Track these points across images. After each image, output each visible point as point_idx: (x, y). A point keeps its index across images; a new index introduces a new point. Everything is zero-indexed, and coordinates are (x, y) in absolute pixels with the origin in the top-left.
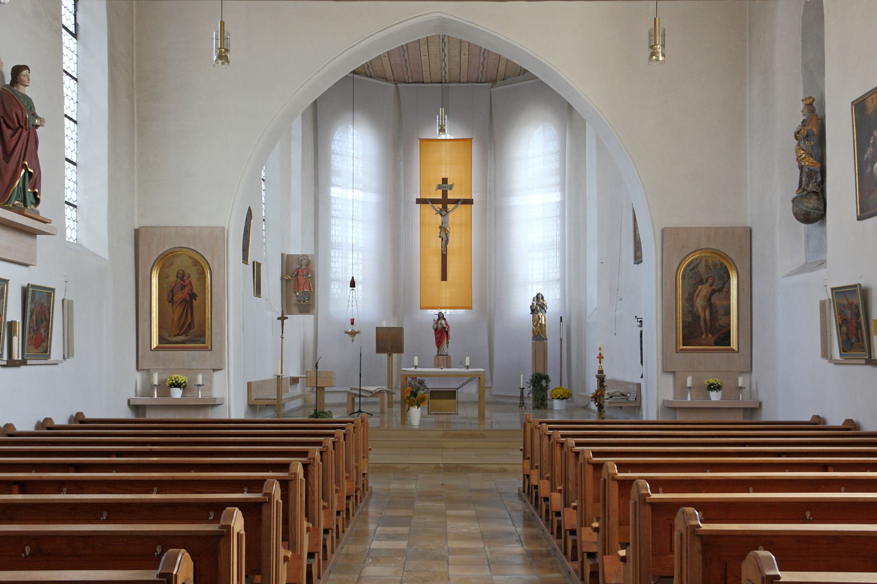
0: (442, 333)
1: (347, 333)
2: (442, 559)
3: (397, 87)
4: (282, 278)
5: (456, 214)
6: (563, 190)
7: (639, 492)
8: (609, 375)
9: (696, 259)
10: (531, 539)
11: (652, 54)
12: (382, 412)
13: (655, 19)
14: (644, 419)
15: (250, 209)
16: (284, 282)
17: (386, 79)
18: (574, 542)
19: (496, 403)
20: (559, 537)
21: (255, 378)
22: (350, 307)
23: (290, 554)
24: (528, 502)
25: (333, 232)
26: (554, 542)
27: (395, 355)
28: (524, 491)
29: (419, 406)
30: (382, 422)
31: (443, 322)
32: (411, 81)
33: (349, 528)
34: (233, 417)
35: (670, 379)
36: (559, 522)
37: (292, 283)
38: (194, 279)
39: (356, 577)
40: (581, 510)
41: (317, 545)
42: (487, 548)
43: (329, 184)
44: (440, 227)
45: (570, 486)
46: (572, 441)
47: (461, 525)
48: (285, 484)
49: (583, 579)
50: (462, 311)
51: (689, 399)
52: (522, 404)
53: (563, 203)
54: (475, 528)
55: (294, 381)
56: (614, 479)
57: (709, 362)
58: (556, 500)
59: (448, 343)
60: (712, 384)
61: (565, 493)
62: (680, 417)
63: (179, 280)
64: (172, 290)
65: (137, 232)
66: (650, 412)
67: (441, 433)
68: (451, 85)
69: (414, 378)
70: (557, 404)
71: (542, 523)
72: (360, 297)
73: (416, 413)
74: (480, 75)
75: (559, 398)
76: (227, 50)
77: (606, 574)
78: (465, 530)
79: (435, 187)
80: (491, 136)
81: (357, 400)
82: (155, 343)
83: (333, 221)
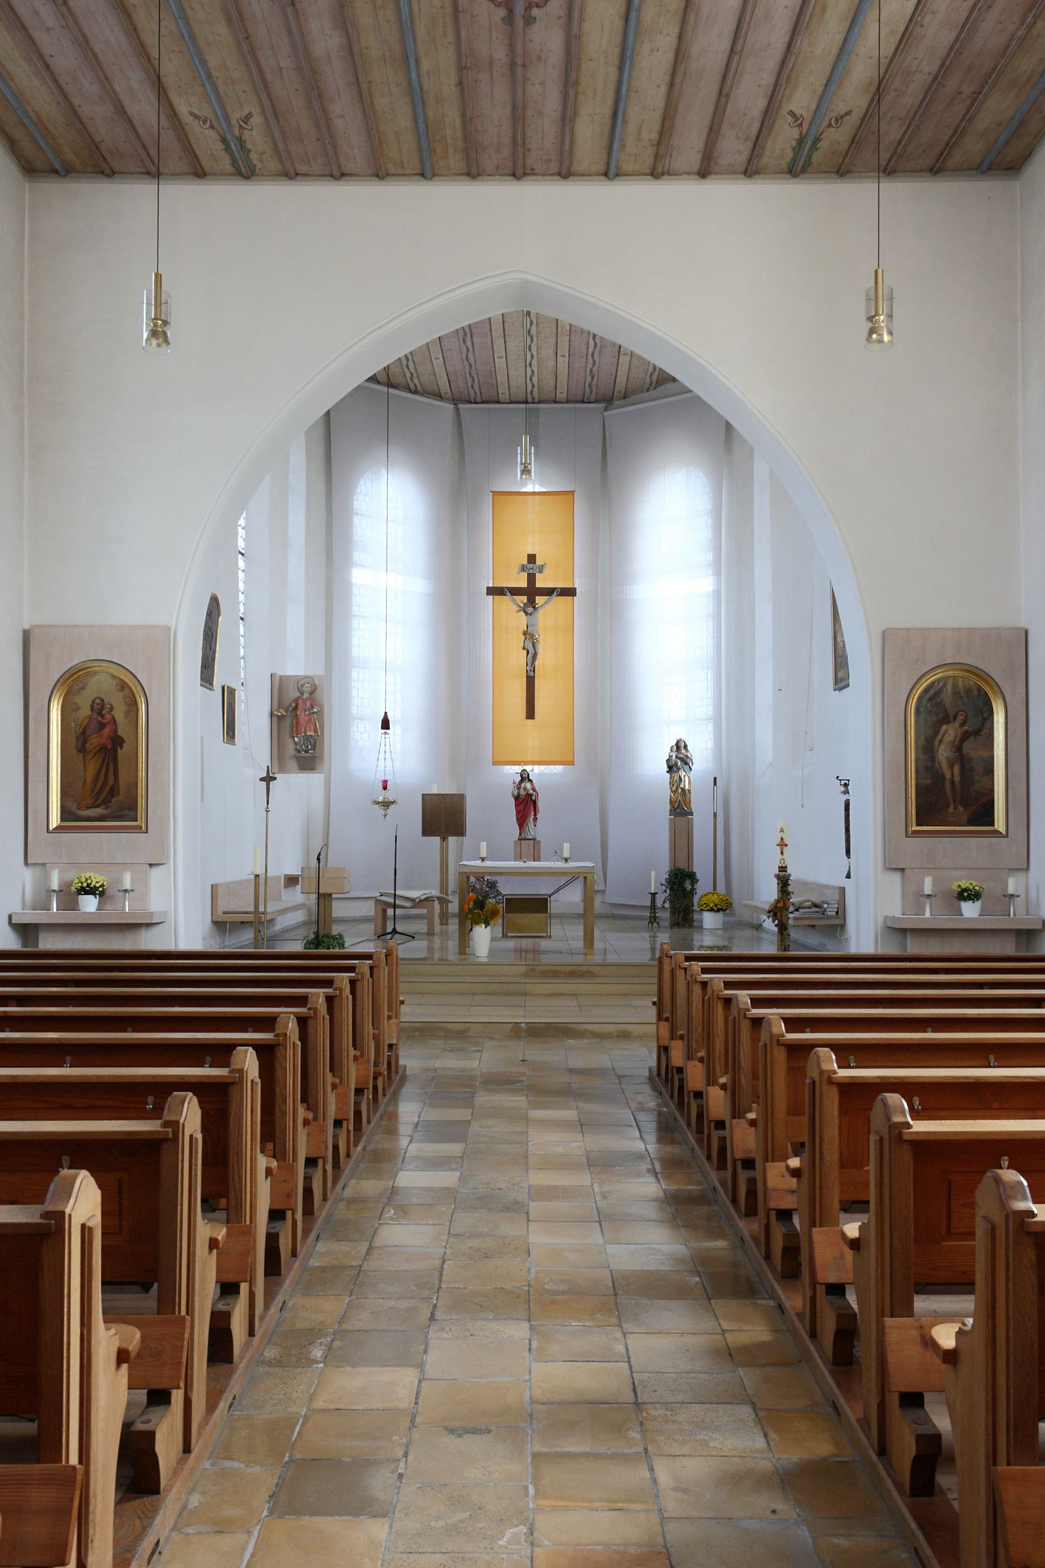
0: (526, 804)
1: (377, 803)
2: (516, 1208)
3: (457, 410)
4: (272, 714)
5: (549, 610)
6: (717, 573)
7: (889, 1119)
8: (795, 873)
9: (939, 680)
10: (671, 1166)
11: (872, 331)
12: (431, 933)
13: (876, 272)
14: (853, 949)
15: (214, 601)
16: (275, 719)
17: (439, 396)
18: (752, 1182)
19: (613, 917)
20: (721, 1166)
21: (224, 876)
22: (382, 760)
23: (221, 1234)
24: (667, 1096)
25: (355, 641)
26: (714, 1176)
27: (452, 840)
28: (659, 1074)
29: (487, 924)
30: (430, 949)
31: (528, 785)
32: (479, 400)
33: (360, 1148)
34: (183, 946)
35: (896, 878)
36: (723, 1140)
37: (288, 721)
38: (119, 714)
39: (364, 1247)
40: (764, 1126)
41: (290, 1195)
42: (596, 1187)
43: (348, 563)
44: (525, 633)
45: (743, 1080)
46: (744, 996)
47: (553, 1138)
48: (266, 1053)
49: (768, 1257)
50: (559, 768)
51: (928, 914)
52: (653, 919)
53: (717, 593)
54: (575, 1144)
55: (291, 881)
56: (831, 1081)
57: (959, 854)
58: (717, 1101)
59: (535, 819)
60: (965, 890)
61: (733, 1090)
62: (914, 947)
63: (95, 715)
64: (84, 732)
65: (26, 635)
66: (863, 937)
67: (523, 969)
68: (541, 406)
69: (480, 878)
70: (709, 920)
71: (691, 1137)
72: (398, 746)
73: (482, 937)
74: (588, 390)
75: (712, 910)
76: (165, 323)
77: (818, 1263)
78: (560, 1150)
79: (517, 568)
80: (604, 483)
81: (390, 912)
82: (55, 821)
83: (355, 623)
